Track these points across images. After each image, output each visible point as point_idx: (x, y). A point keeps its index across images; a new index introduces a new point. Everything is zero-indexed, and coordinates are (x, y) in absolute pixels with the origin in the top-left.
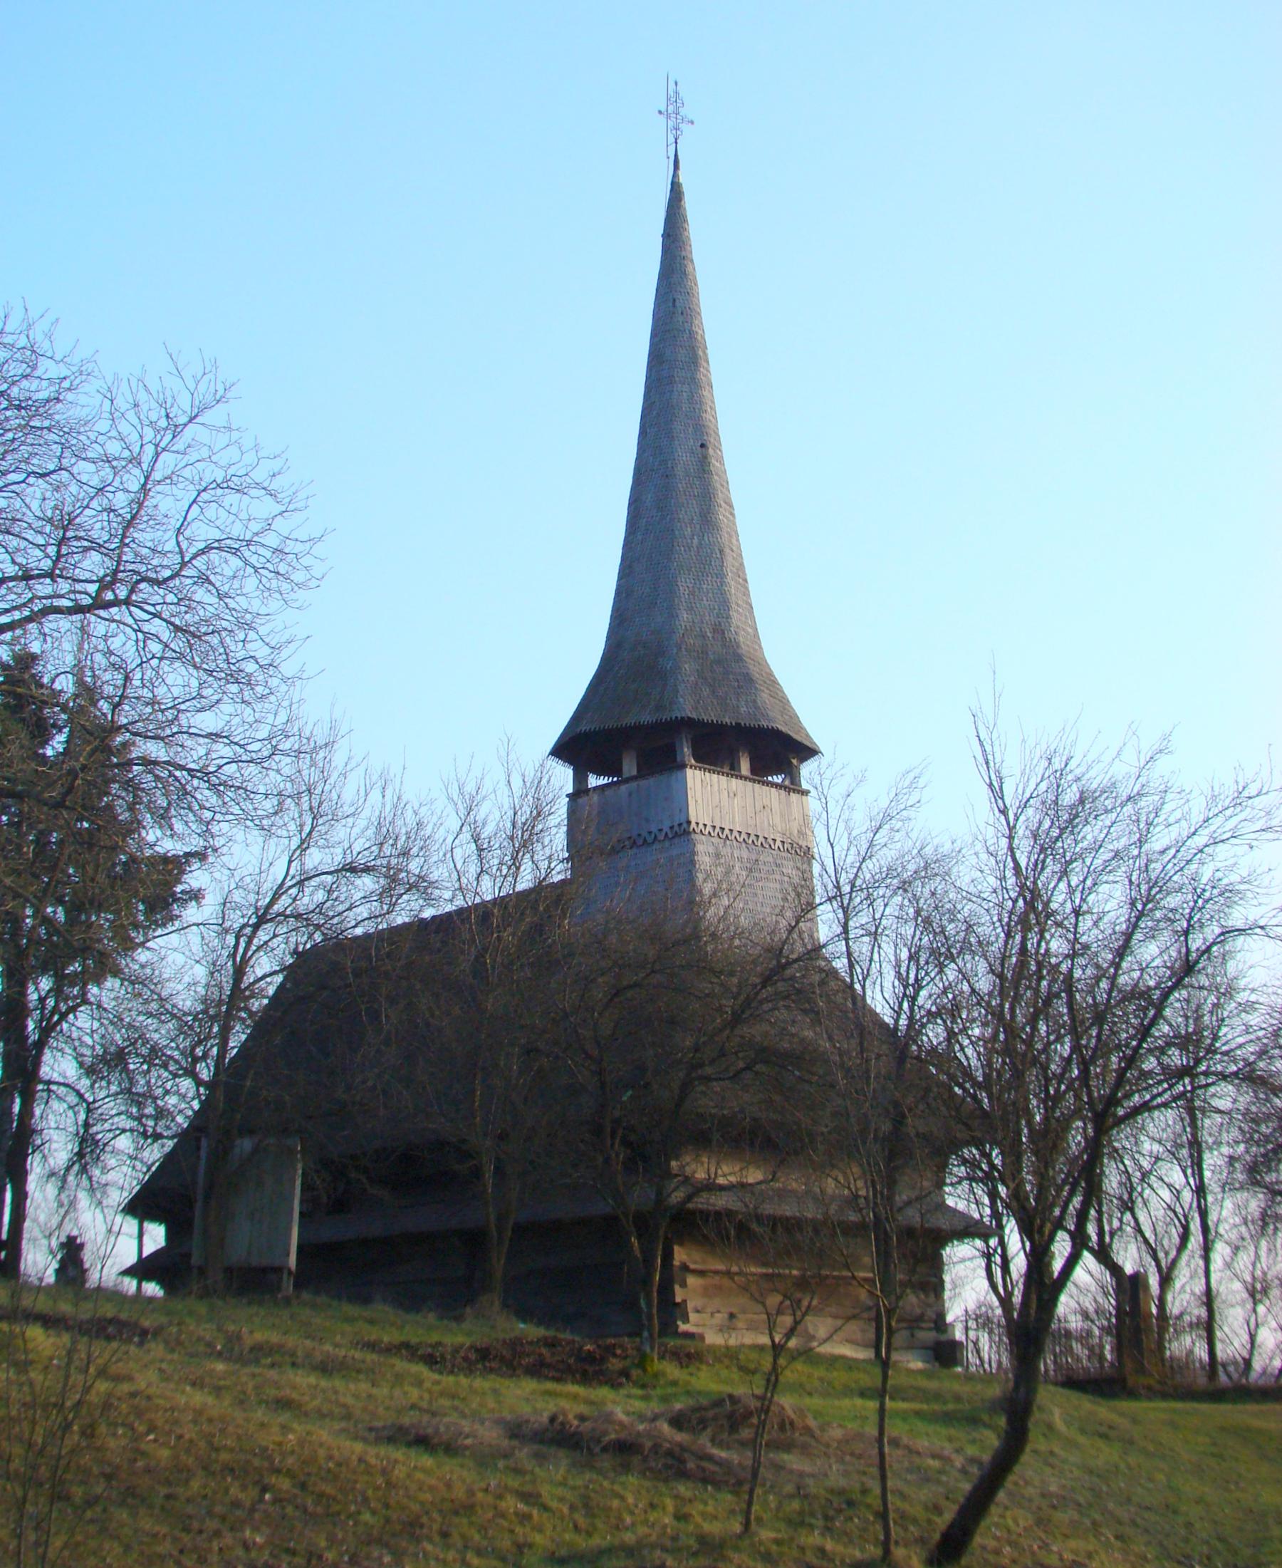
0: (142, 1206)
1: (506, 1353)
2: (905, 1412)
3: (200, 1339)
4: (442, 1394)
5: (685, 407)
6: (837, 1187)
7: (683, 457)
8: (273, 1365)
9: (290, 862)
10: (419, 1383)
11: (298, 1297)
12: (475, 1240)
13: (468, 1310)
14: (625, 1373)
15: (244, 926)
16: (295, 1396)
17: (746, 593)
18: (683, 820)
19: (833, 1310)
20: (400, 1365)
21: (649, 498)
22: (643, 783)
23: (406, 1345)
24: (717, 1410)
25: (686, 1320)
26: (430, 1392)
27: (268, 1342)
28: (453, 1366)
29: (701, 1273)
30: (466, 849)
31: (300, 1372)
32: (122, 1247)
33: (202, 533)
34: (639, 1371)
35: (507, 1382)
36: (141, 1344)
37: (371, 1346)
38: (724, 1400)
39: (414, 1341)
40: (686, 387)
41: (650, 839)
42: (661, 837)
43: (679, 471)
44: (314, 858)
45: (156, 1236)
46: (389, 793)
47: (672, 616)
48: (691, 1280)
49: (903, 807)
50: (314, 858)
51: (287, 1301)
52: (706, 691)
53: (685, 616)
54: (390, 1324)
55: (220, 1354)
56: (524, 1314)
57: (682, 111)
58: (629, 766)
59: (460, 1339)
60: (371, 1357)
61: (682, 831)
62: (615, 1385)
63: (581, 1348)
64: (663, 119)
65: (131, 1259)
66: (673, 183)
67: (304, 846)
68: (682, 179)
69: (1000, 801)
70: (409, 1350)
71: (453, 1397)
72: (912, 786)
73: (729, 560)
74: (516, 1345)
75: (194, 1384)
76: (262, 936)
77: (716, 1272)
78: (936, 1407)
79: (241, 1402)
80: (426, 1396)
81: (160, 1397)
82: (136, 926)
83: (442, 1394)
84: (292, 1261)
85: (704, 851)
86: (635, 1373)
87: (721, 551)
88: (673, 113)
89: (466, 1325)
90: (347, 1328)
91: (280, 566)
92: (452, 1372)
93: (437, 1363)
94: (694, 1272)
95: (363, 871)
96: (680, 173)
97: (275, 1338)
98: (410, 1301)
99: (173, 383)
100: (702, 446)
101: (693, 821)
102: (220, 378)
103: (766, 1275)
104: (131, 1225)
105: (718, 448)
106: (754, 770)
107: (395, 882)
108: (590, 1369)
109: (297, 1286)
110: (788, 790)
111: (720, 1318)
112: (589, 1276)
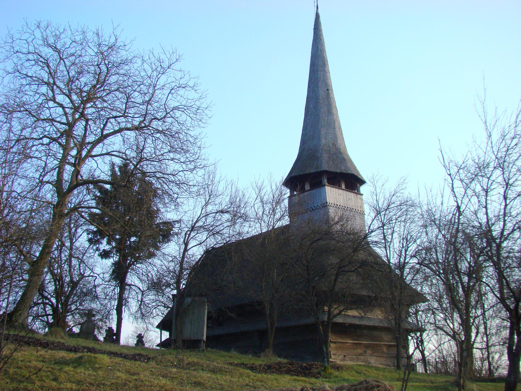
0: (163, 326)
1: (277, 367)
3: (169, 361)
4: (257, 380)
6: (377, 316)
7: (322, 93)
8: (195, 370)
9: (202, 209)
10: (249, 376)
12: (263, 334)
13: (262, 354)
14: (319, 373)
15: (188, 231)
16: (202, 381)
17: (342, 134)
18: (325, 202)
19: (376, 354)
20: (242, 370)
21: (311, 106)
22: (312, 191)
23: (243, 364)
24: (360, 386)
26: (252, 379)
28: (260, 371)
29: (335, 343)
30: (258, 205)
31: (205, 372)
32: (155, 337)
33: (172, 103)
34: (324, 373)
36: (147, 362)
37: (231, 364)
39: (245, 363)
40: (322, 73)
41: (315, 209)
43: (321, 97)
44: (210, 208)
45: (166, 335)
46: (233, 188)
47: (319, 139)
48: (332, 345)
49: (400, 189)
50: (210, 208)
51: (203, 351)
52: (331, 163)
53: (323, 141)
54: (236, 357)
55: (176, 366)
56: (279, 356)
58: (307, 187)
59: (261, 363)
60: (231, 367)
61: (325, 205)
62: (317, 378)
63: (302, 365)
68: (319, 12)
69: (448, 171)
70: (244, 365)
71: (261, 381)
72: (403, 183)
73: (336, 124)
74: (279, 363)
75: (163, 376)
76: (193, 234)
78: (422, 384)
79: (181, 384)
80: (251, 381)
81: (146, 381)
82: (160, 242)
83: (257, 380)
84: (205, 338)
85: (332, 211)
86: (322, 373)
87: (334, 121)
89: (262, 359)
90: (223, 359)
91: (196, 112)
92: (260, 373)
93: (254, 369)
94: (333, 342)
95: (225, 212)
97: (196, 360)
98: (244, 351)
99: (163, 57)
100: (328, 90)
101: (328, 202)
102: (178, 53)
103: (354, 343)
104: (158, 330)
105: (332, 91)
106: (346, 187)
107: (236, 215)
108: (307, 372)
109: (207, 346)
110: (357, 194)
112: (302, 345)
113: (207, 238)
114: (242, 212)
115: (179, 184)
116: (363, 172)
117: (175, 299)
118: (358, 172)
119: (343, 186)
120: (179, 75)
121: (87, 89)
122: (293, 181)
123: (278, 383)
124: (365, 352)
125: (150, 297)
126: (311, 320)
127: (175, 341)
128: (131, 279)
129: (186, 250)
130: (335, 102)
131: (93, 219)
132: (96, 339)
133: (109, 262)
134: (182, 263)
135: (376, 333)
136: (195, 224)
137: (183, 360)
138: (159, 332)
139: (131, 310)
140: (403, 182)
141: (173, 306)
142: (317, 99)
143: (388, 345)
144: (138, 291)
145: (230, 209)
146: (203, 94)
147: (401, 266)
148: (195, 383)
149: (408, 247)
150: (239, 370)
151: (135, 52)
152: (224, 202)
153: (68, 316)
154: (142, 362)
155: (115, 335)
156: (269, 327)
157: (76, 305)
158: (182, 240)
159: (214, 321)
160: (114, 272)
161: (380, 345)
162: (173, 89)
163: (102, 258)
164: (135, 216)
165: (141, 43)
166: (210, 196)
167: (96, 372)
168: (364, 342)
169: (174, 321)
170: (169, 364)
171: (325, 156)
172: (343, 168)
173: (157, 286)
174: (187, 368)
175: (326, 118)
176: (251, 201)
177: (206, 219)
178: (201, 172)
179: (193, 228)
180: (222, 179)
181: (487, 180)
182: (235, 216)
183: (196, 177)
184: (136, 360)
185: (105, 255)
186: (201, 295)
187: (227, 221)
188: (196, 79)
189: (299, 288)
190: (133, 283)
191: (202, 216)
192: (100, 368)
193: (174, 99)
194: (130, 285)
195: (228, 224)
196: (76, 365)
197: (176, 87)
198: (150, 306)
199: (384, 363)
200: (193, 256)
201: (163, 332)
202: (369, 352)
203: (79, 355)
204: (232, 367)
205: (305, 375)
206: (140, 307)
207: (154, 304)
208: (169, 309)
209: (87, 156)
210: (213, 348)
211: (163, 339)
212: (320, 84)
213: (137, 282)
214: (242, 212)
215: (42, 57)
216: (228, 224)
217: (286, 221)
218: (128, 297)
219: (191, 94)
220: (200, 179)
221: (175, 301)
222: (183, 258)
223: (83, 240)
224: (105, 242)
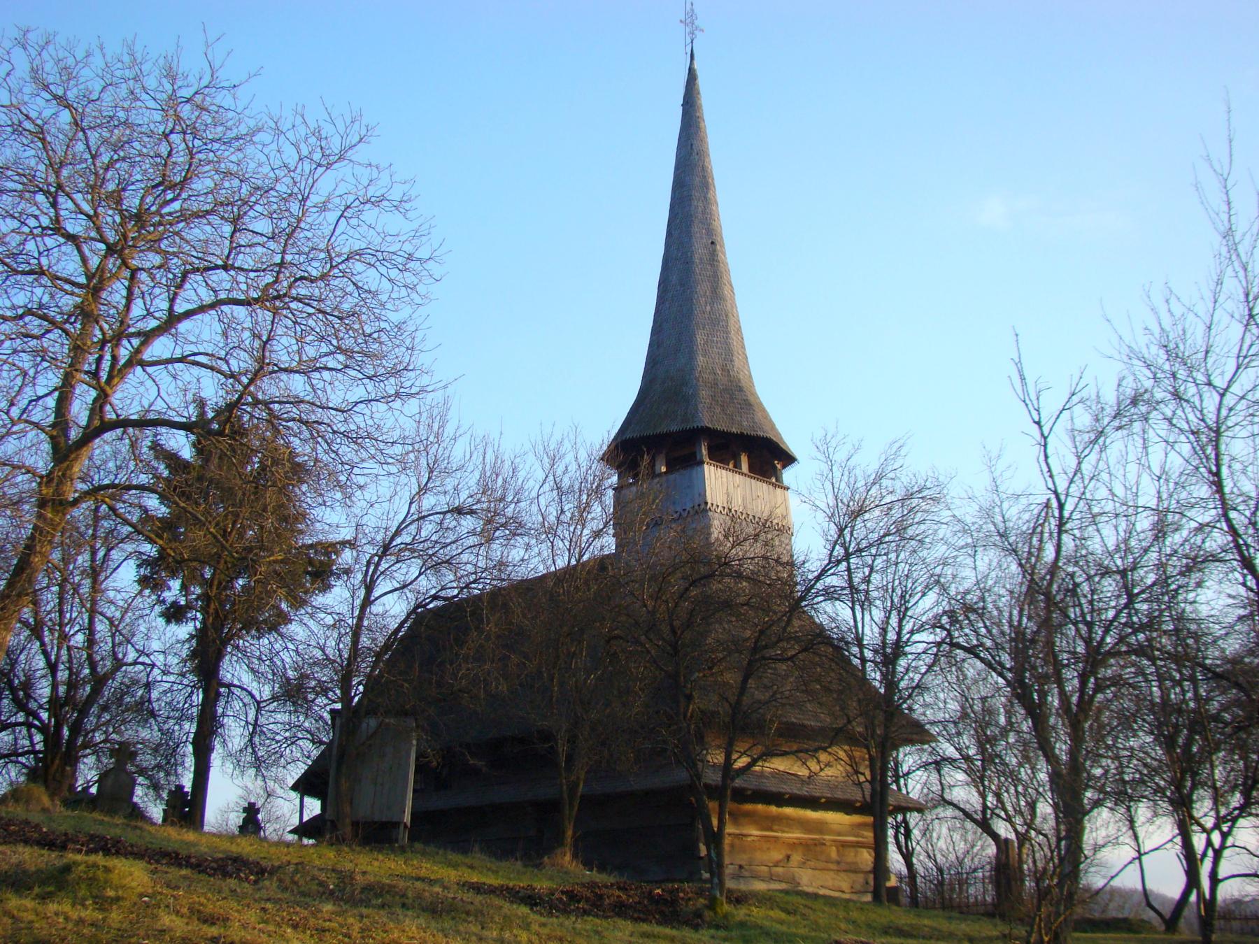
0: (305, 786)
3: (313, 878)
5: (700, 216)
7: (699, 250)
8: (383, 906)
9: (411, 503)
11: (412, 847)
17: (743, 347)
19: (812, 864)
21: (674, 279)
22: (671, 477)
27: (379, 882)
31: (410, 913)
32: (288, 810)
33: (344, 245)
34: (711, 913)
35: (605, 923)
36: (256, 882)
42: (685, 514)
44: (428, 502)
45: (314, 807)
47: (691, 357)
50: (428, 502)
51: (403, 850)
52: (718, 410)
53: (701, 360)
55: (332, 893)
56: (602, 869)
57: (696, 23)
61: (701, 509)
62: (696, 927)
63: (650, 892)
64: (683, 25)
65: (295, 821)
66: (690, 69)
67: (423, 490)
73: (732, 321)
84: (407, 818)
86: (708, 914)
88: (689, 20)
93: (536, 904)
98: (501, 850)
99: (327, 130)
101: (709, 502)
102: (364, 122)
104: (294, 795)
105: (722, 246)
106: (751, 469)
107: (496, 519)
109: (413, 838)
110: (775, 486)
113: (420, 574)
114: (510, 511)
115: (354, 439)
116: (791, 437)
117: (338, 721)
118: (778, 434)
119: (731, 466)
120: (365, 174)
121: (134, 199)
124: (788, 857)
125: (278, 719)
126: (681, 776)
127: (334, 826)
128: (233, 670)
129: (367, 602)
130: (728, 272)
131: (147, 527)
132: (137, 814)
133: (184, 631)
134: (356, 632)
136: (392, 539)
138: (298, 801)
139: (230, 745)
140: (896, 451)
141: (331, 741)
142: (688, 262)
144: (247, 699)
145: (478, 506)
146: (423, 228)
147: (891, 654)
149: (907, 609)
151: (259, 117)
152: (467, 487)
153: (85, 756)
154: (240, 879)
155: (188, 803)
156: (565, 796)
157: (105, 732)
158: (360, 576)
159: (431, 777)
160: (194, 654)
162: (349, 207)
163: (168, 622)
164: (250, 528)
165: (273, 90)
166: (431, 471)
167: (101, 909)
169: (332, 773)
170: (315, 887)
171: (704, 393)
173: (293, 692)
174: (361, 901)
175: (708, 308)
176: (532, 486)
177: (419, 530)
178: (412, 406)
179: (386, 548)
180: (461, 431)
181: (1217, 398)
182: (489, 522)
183: (397, 420)
184: (226, 875)
185: (174, 614)
187: (473, 533)
188: (407, 187)
189: (624, 703)
190: (236, 682)
191: (409, 520)
192: (118, 899)
193: (351, 232)
194: (229, 685)
195: (473, 540)
196: (51, 889)
197: (357, 203)
198: (278, 738)
200: (383, 615)
201: (307, 800)
205: (665, 920)
206: (250, 740)
207: (287, 734)
208: (323, 747)
209: (130, 363)
210: (427, 842)
212: (695, 229)
213: (246, 679)
214: (510, 511)
215: (28, 117)
216: (473, 540)
217: (608, 544)
218: (224, 715)
219: (392, 222)
220: (409, 427)
221: (337, 728)
222: (361, 618)
223: (124, 578)
224: (176, 584)
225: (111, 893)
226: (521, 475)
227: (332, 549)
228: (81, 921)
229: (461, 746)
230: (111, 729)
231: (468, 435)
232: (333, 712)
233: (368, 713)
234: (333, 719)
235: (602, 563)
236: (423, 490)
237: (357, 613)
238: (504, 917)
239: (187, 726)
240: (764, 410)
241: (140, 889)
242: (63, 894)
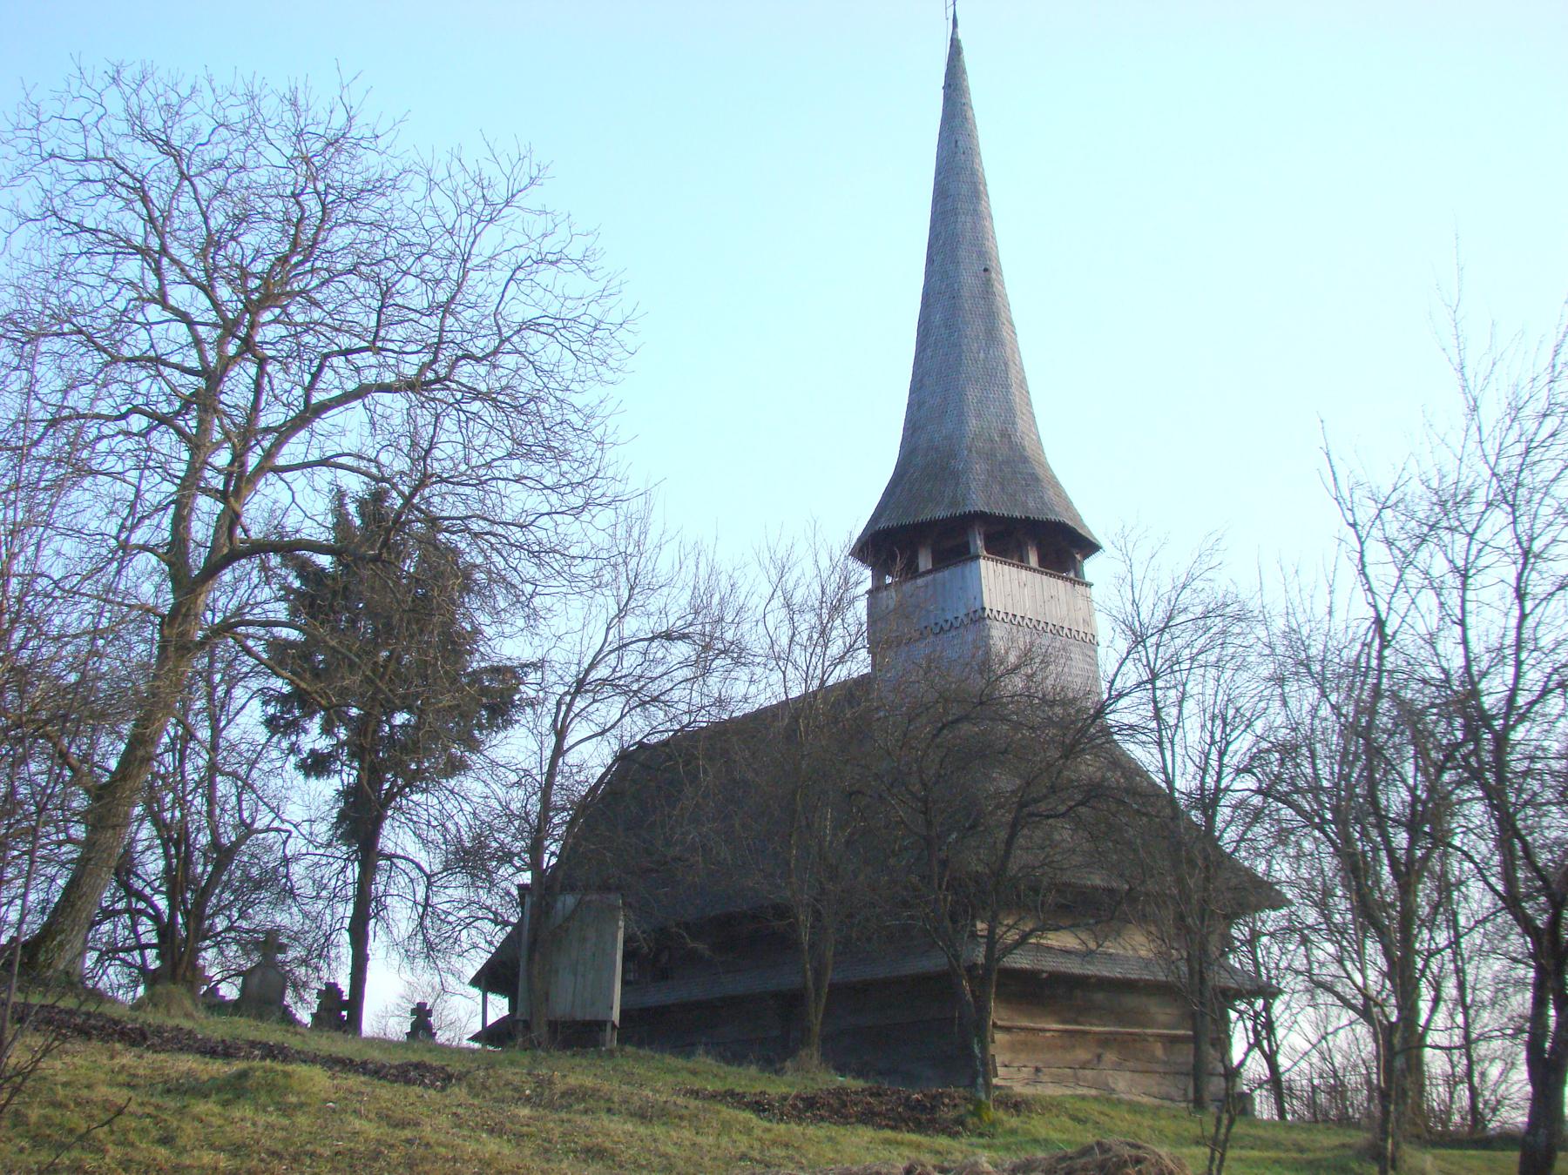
0: (490, 979)
1: (835, 1102)
2: (1263, 1160)
3: (507, 1084)
4: (774, 1143)
6: (1133, 951)
7: (968, 280)
8: (586, 1112)
9: (608, 629)
10: (748, 1131)
12: (791, 1003)
13: (788, 1063)
14: (960, 1121)
15: (566, 693)
16: (608, 1144)
17: (1029, 404)
18: (978, 606)
19: (1130, 1064)
20: (727, 1112)
21: (937, 319)
22: (939, 575)
25: (996, 1076)
26: (760, 1139)
28: (782, 1114)
29: (1008, 1029)
30: (777, 615)
31: (615, 1118)
32: (467, 1013)
33: (518, 311)
34: (976, 1120)
35: (842, 1131)
36: (443, 1089)
37: (695, 1094)
38: (1092, 1148)
40: (969, 219)
41: (946, 627)
43: (965, 293)
44: (631, 625)
45: (499, 1007)
46: (703, 560)
47: (961, 419)
50: (631, 625)
51: (611, 1053)
53: (973, 424)
54: (710, 1072)
55: (528, 1099)
56: (841, 1070)
58: (925, 562)
59: (784, 1090)
60: (694, 1103)
61: (978, 617)
62: (954, 1135)
63: (908, 1098)
67: (622, 613)
68: (961, 35)
69: (1348, 514)
70: (733, 1098)
73: (1013, 371)
74: (840, 1092)
75: (491, 1131)
76: (580, 704)
77: (1022, 1029)
78: (1272, 1154)
79: (546, 1152)
80: (757, 1145)
82: (481, 727)
83: (774, 1143)
84: (616, 1016)
85: (998, 634)
87: (1006, 364)
89: (788, 1078)
90: (669, 1078)
91: (589, 335)
93: (764, 1110)
94: (1002, 1028)
95: (678, 638)
96: (960, 30)
97: (589, 1082)
98: (734, 1056)
99: (490, 171)
100: (986, 270)
102: (535, 160)
103: (1066, 1031)
104: (476, 993)
105: (999, 273)
106: (1042, 562)
107: (712, 646)
108: (924, 1117)
110: (1074, 582)
111: (1027, 1072)
112: (909, 1037)
113: (622, 716)
115: (537, 554)
117: (528, 899)
118: (1077, 517)
119: (1033, 560)
120: (539, 225)
121: (262, 269)
122: (882, 545)
123: (838, 1152)
124: (1099, 1057)
125: (453, 892)
126: (936, 962)
127: (528, 1026)
128: (395, 837)
129: (559, 751)
130: (1007, 306)
133: (327, 788)
134: (546, 790)
135: (1131, 1001)
136: (587, 672)
137: (551, 1082)
138: (480, 999)
139: (395, 931)
141: (521, 920)
142: (955, 297)
143: (1167, 1036)
144: (415, 873)
145: (691, 629)
147: (1208, 801)
148: (588, 1150)
150: (719, 1112)
152: (673, 606)
153: (205, 949)
154: (426, 1086)
156: (810, 984)
157: (229, 917)
159: (643, 963)
160: (342, 816)
161: (1143, 1038)
162: (519, 268)
163: (307, 775)
164: (407, 650)
165: (423, 128)
166: (632, 588)
168: (1095, 1029)
169: (523, 964)
170: (508, 1093)
171: (979, 468)
172: (1031, 504)
173: (471, 858)
176: (757, 603)
177: (620, 659)
178: (604, 517)
179: (580, 686)
183: (588, 534)
184: (409, 1082)
185: (316, 765)
186: (605, 888)
187: (685, 663)
188: (591, 239)
189: (892, 869)
190: (400, 852)
191: (606, 649)
192: (302, 1105)
194: (390, 857)
195: (687, 672)
197: (529, 262)
198: (451, 918)
199: (1155, 1090)
201: (490, 996)
202: (1110, 1057)
203: (238, 1066)
204: (699, 1103)
205: (920, 1128)
206: (421, 924)
208: (509, 929)
209: (261, 470)
210: (640, 1045)
211: (492, 1019)
212: (962, 253)
213: (412, 847)
214: (729, 636)
215: (125, 171)
216: (687, 672)
217: (860, 664)
218: (386, 894)
219: (572, 283)
220: (601, 539)
221: (527, 906)
223: (248, 722)
224: (315, 725)
225: (294, 1099)
226: (742, 591)
227: (509, 675)
228: (268, 1126)
229: (678, 925)
230: (236, 915)
231: (677, 539)
232: (521, 887)
233: (563, 890)
234: (521, 896)
235: (855, 689)
236: (622, 613)
237: (545, 769)
238: (723, 1123)
239: (340, 909)
240: (1057, 485)
241: (323, 1095)
242: (242, 1101)
